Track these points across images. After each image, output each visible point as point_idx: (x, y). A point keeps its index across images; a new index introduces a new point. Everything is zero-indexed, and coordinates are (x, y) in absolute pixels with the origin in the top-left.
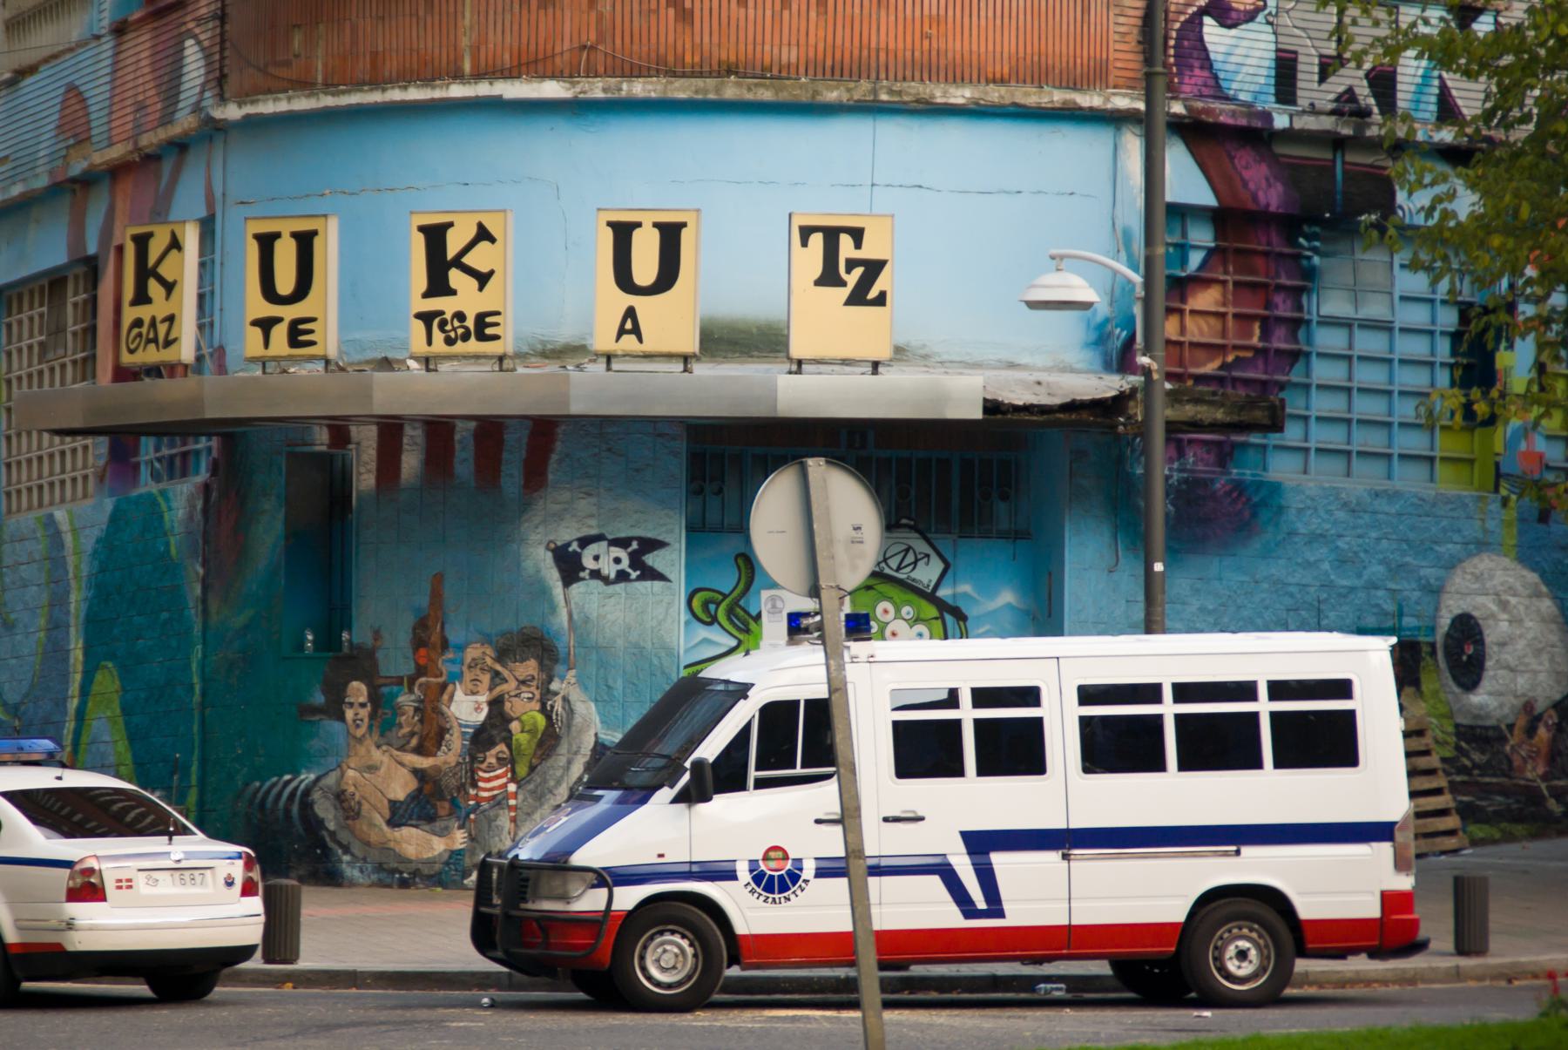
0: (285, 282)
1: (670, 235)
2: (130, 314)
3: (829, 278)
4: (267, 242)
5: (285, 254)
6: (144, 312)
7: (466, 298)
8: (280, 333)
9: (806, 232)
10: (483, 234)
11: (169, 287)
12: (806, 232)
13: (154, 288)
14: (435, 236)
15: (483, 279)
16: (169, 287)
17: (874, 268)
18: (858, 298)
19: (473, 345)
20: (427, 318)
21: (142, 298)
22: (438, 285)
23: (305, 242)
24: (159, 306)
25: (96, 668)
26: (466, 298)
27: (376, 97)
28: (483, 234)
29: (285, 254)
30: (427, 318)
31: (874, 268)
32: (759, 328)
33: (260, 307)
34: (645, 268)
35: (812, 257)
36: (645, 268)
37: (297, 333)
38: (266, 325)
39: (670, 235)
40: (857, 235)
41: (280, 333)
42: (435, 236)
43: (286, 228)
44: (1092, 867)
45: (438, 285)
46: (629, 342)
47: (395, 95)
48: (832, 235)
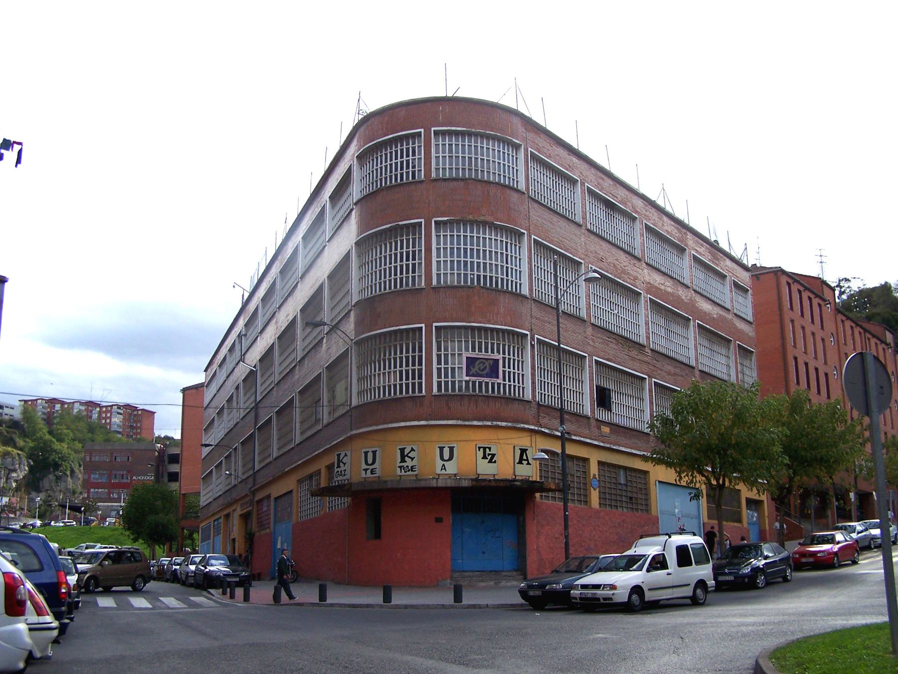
0: (370, 461)
1: (451, 449)
2: (336, 470)
3: (484, 457)
4: (366, 453)
5: (370, 456)
6: (339, 469)
7: (409, 463)
8: (369, 471)
9: (479, 448)
10: (412, 450)
11: (345, 464)
12: (479, 448)
13: (341, 464)
14: (402, 450)
15: (412, 459)
16: (345, 464)
17: (493, 455)
18: (490, 461)
19: (410, 473)
20: (400, 467)
21: (339, 466)
22: (403, 461)
23: (374, 453)
24: (342, 468)
25: (872, 454)
26: (409, 463)
27: (386, 426)
28: (412, 450)
29: (370, 456)
30: (400, 467)
31: (493, 455)
32: (246, 542)
33: (364, 466)
34: (446, 456)
35: (480, 454)
36: (446, 456)
37: (372, 472)
38: (366, 470)
39: (451, 449)
40: (490, 449)
41: (369, 471)
42: (402, 450)
43: (370, 450)
44: (675, 590)
45: (403, 461)
46: (443, 472)
47: (391, 426)
48: (485, 449)
